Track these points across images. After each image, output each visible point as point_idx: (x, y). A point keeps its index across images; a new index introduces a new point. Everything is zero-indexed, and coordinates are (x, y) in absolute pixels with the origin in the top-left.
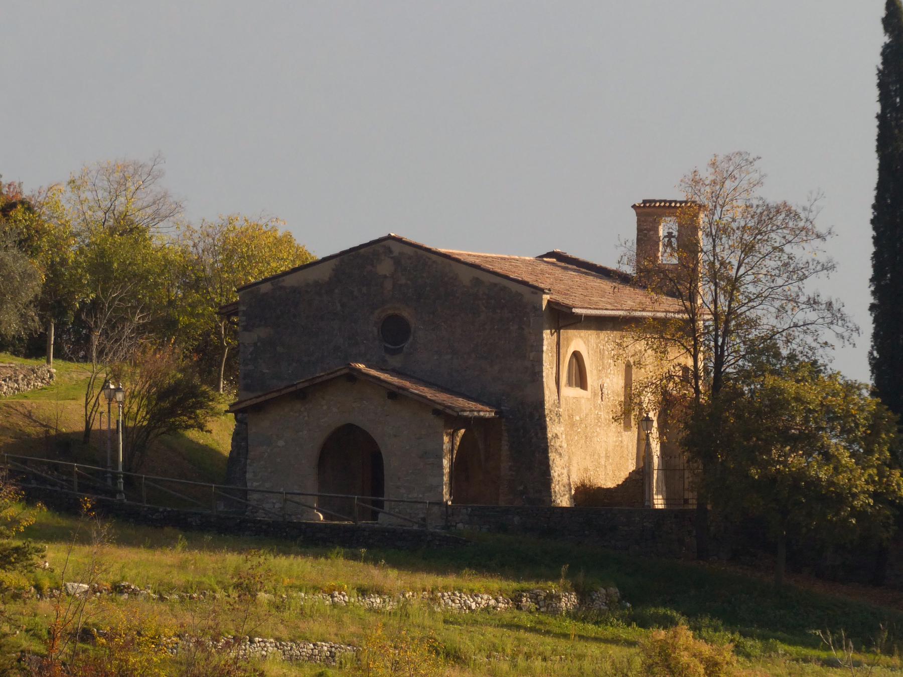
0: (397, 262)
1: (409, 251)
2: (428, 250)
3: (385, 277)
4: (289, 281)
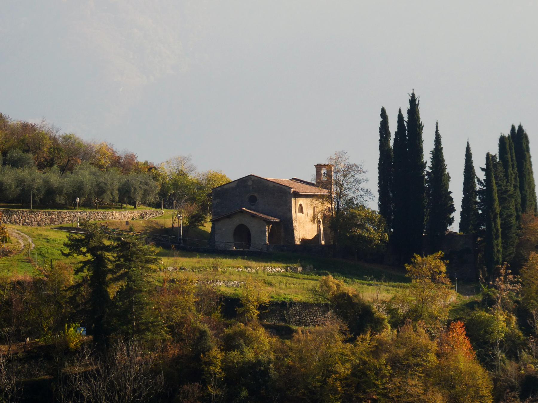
0: (253, 181)
1: (257, 178)
2: (261, 178)
3: (250, 185)
4: (225, 187)
